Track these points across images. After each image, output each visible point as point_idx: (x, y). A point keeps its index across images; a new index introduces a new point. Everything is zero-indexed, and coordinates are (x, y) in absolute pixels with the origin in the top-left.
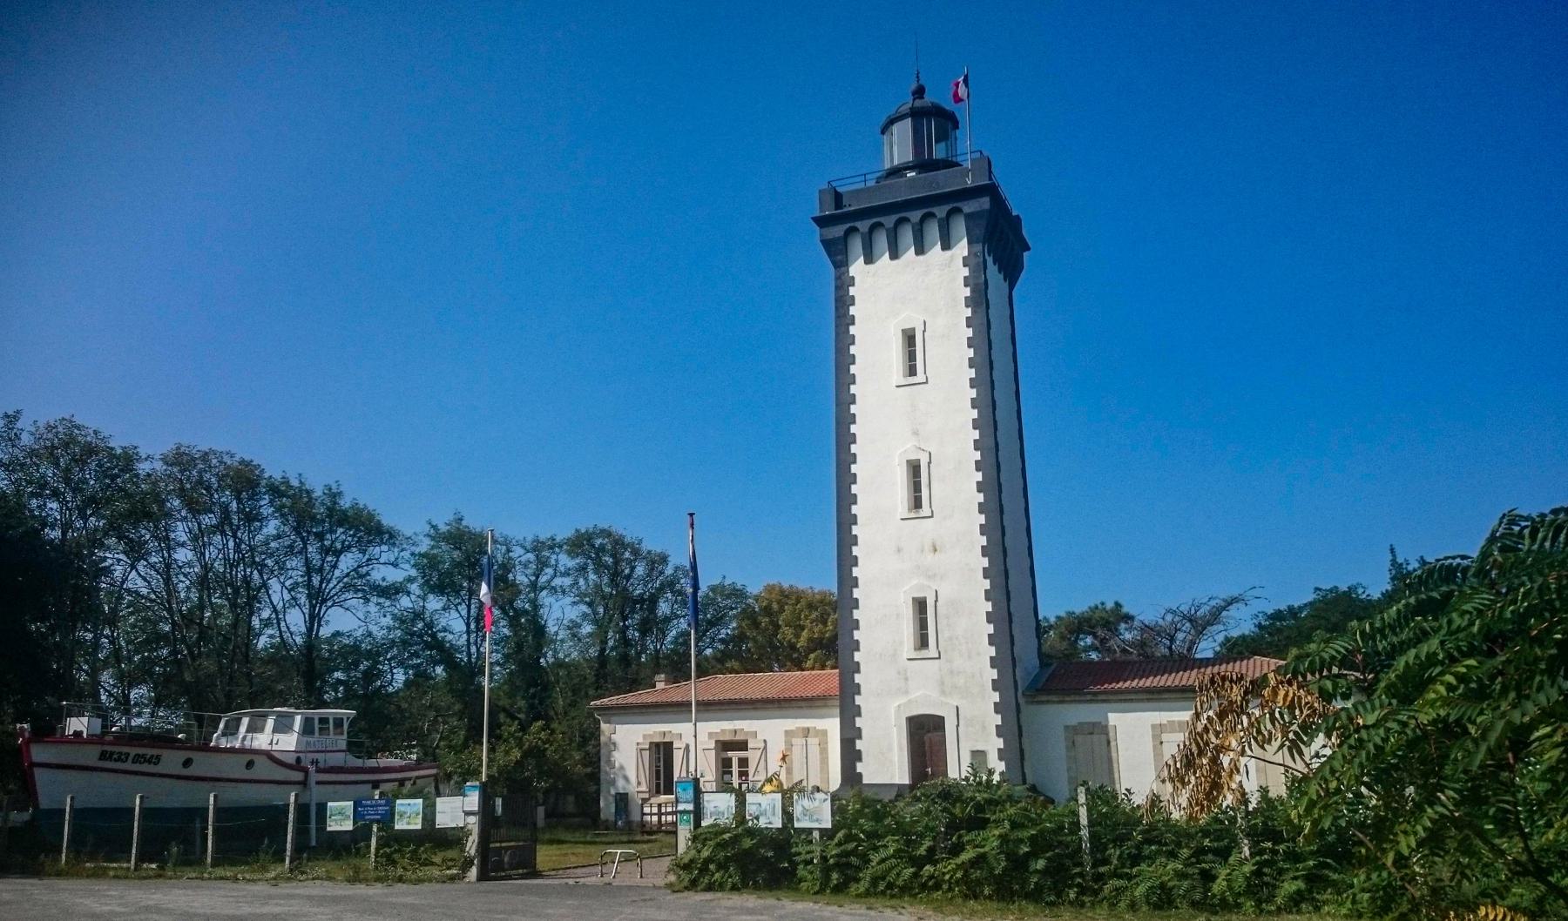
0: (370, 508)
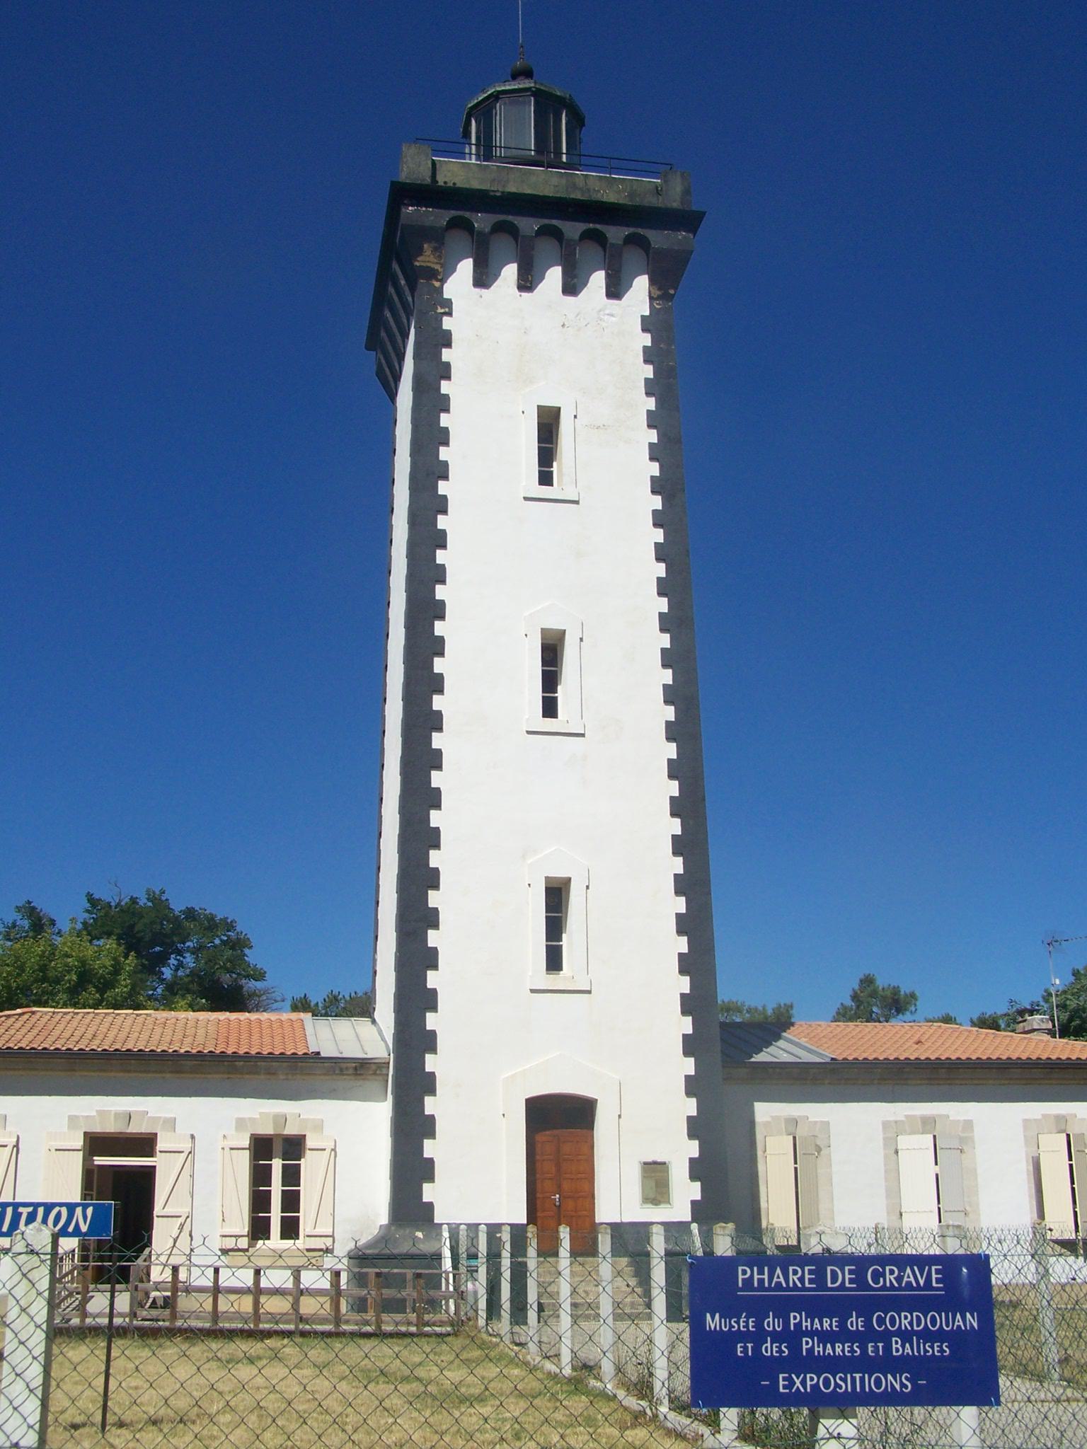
0: (734, 1000)
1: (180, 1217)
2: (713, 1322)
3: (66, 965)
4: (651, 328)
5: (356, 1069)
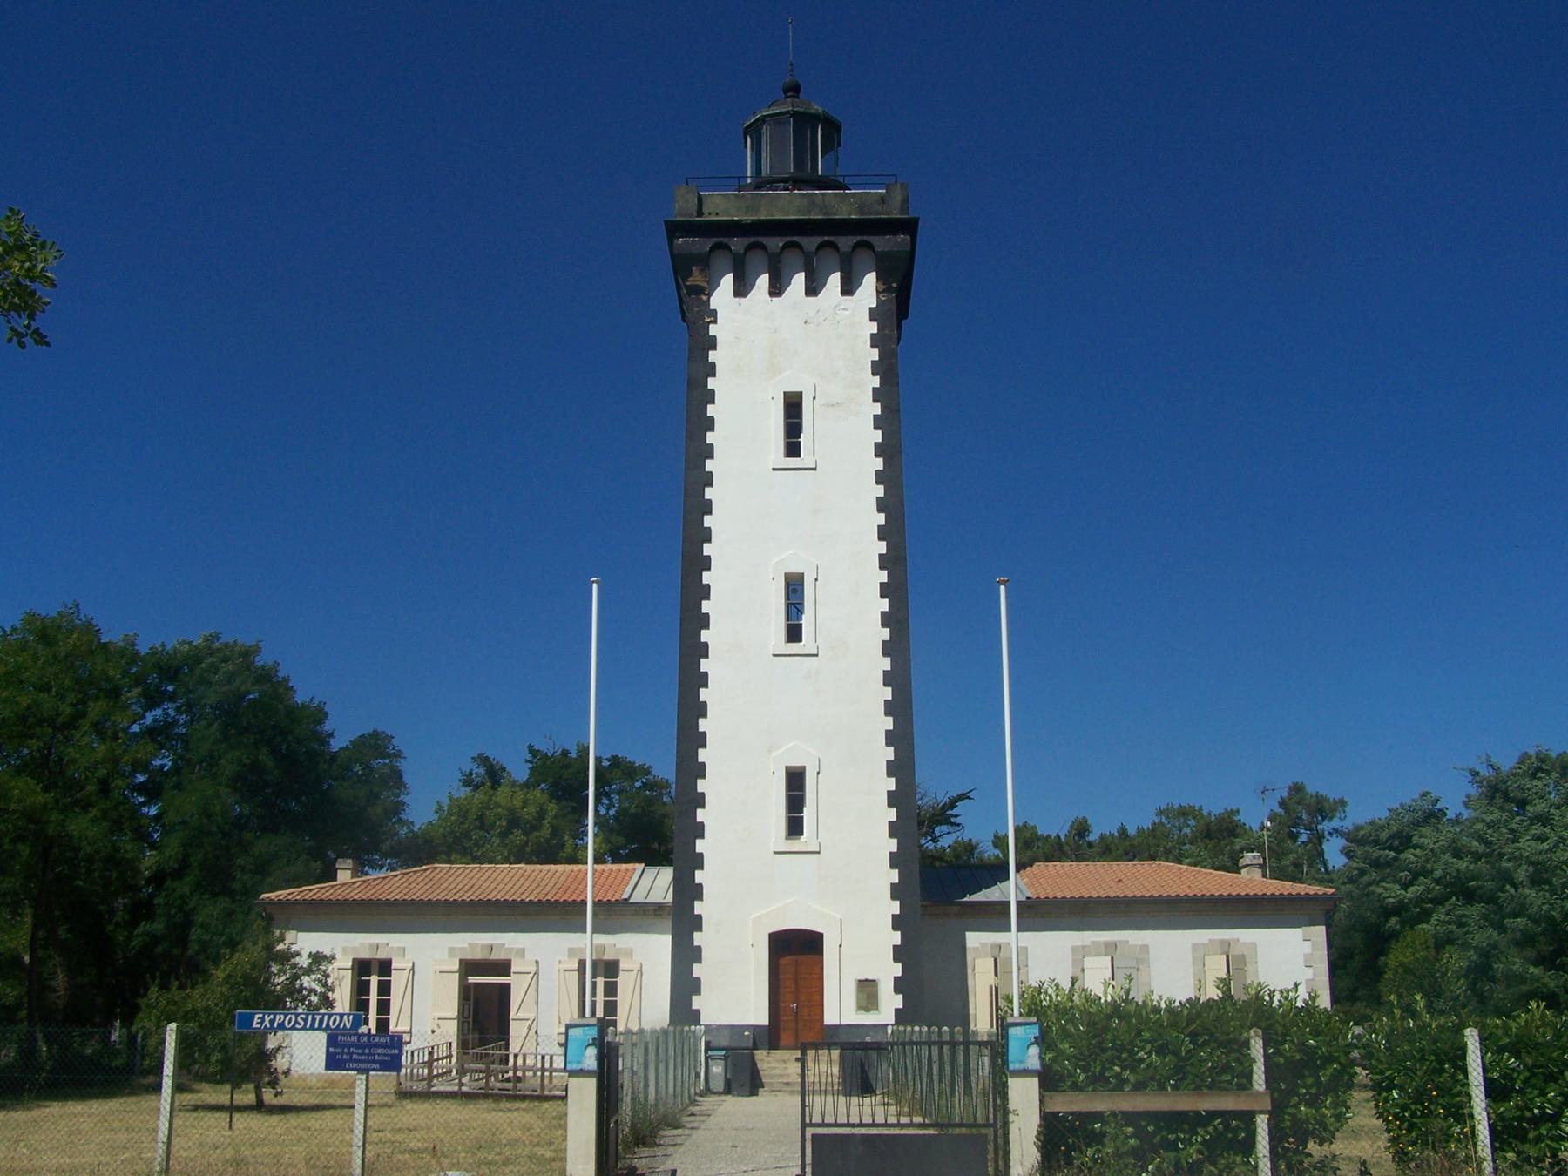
1: (528, 1020)
2: (331, 1050)
3: (498, 814)
4: (877, 317)
5: (655, 910)
